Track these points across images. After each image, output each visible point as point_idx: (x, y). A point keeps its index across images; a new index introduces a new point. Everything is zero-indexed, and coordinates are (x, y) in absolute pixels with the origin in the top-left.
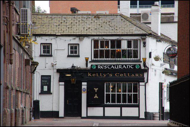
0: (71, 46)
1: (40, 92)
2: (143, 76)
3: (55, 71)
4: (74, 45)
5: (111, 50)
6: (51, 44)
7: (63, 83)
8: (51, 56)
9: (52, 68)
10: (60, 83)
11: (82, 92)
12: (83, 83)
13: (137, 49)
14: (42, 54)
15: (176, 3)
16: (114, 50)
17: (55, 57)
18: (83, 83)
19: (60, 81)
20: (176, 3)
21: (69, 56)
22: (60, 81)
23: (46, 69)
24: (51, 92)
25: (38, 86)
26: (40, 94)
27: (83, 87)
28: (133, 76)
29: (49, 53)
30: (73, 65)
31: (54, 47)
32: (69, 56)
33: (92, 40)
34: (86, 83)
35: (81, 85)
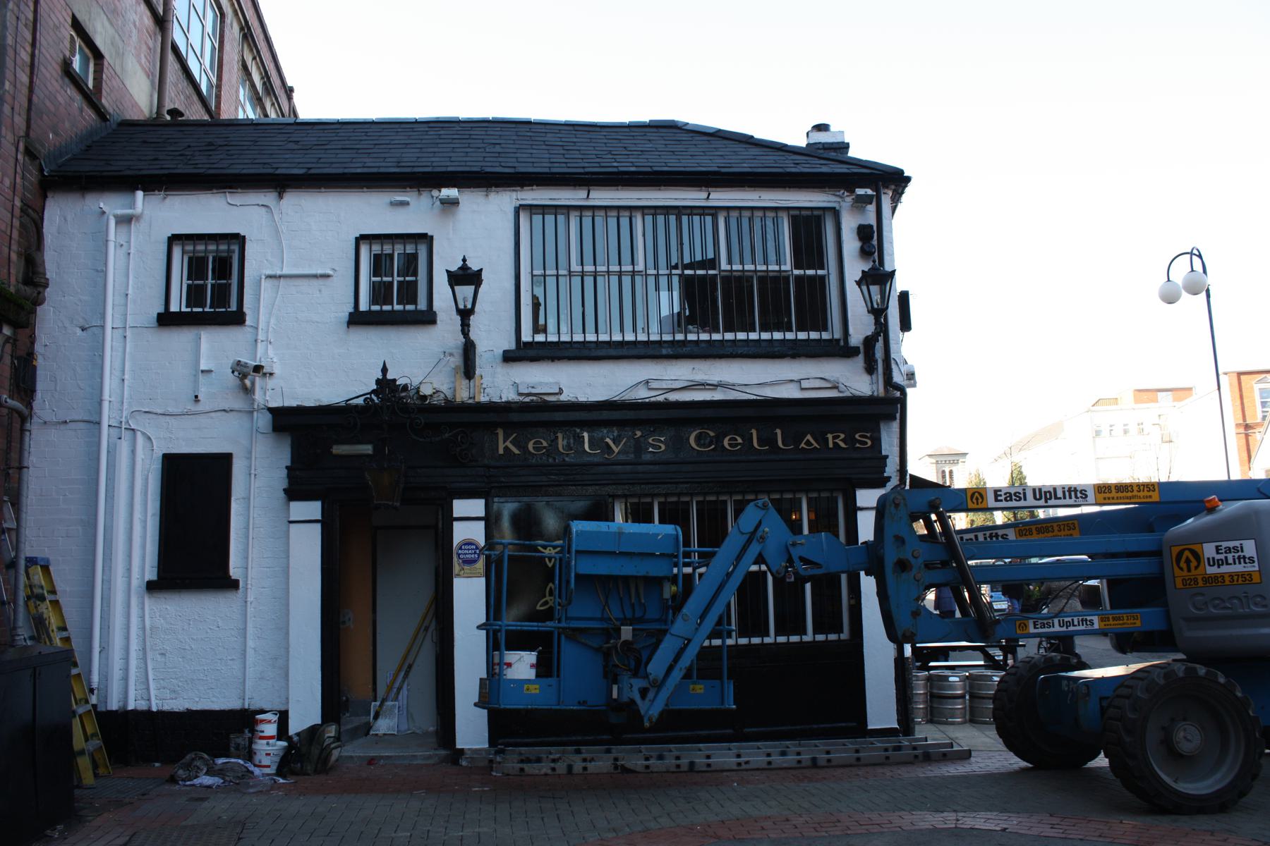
0: (376, 248)
1: (151, 575)
2: (877, 442)
3: (264, 421)
4: (399, 249)
5: (798, 278)
6: (239, 239)
7: (313, 509)
8: (237, 319)
9: (238, 403)
10: (294, 505)
11: (456, 568)
12: (461, 507)
13: (389, 279)
14: (363, 306)
15: (800, 447)
16: (816, 276)
17: (262, 325)
18: (461, 507)
19: (294, 493)
20: (800, 447)
21: (357, 319)
22: (294, 493)
23: (200, 408)
24: (234, 571)
25: (137, 515)
26: (152, 587)
27: (461, 532)
28: (808, 443)
29: (414, 302)
30: (384, 370)
31: (257, 262)
32: (357, 319)
33: (517, 211)
34: (476, 507)
35: (450, 520)
